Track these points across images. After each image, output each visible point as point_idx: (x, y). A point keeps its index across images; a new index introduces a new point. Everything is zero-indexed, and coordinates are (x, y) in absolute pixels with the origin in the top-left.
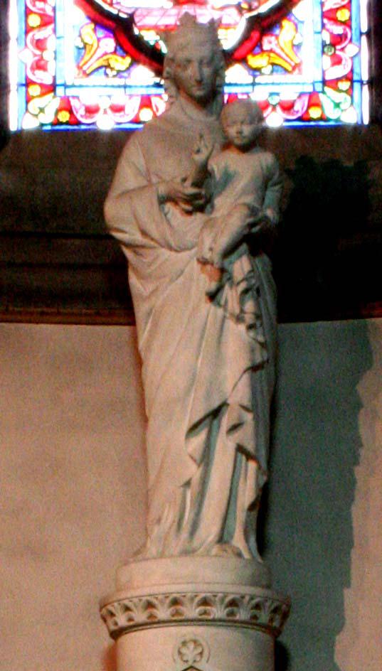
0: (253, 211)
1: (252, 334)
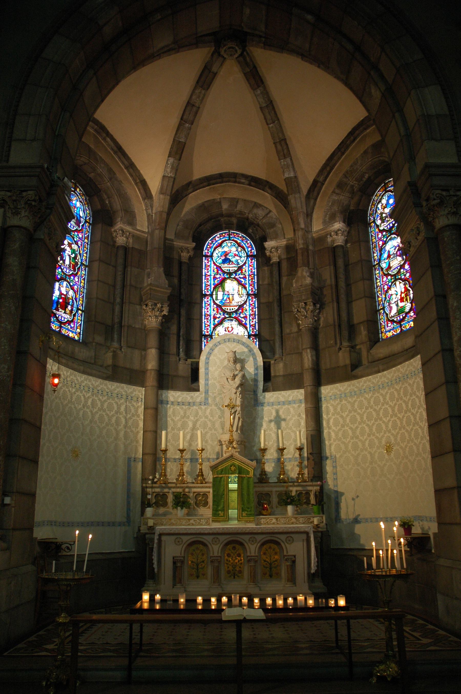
0: (241, 381)
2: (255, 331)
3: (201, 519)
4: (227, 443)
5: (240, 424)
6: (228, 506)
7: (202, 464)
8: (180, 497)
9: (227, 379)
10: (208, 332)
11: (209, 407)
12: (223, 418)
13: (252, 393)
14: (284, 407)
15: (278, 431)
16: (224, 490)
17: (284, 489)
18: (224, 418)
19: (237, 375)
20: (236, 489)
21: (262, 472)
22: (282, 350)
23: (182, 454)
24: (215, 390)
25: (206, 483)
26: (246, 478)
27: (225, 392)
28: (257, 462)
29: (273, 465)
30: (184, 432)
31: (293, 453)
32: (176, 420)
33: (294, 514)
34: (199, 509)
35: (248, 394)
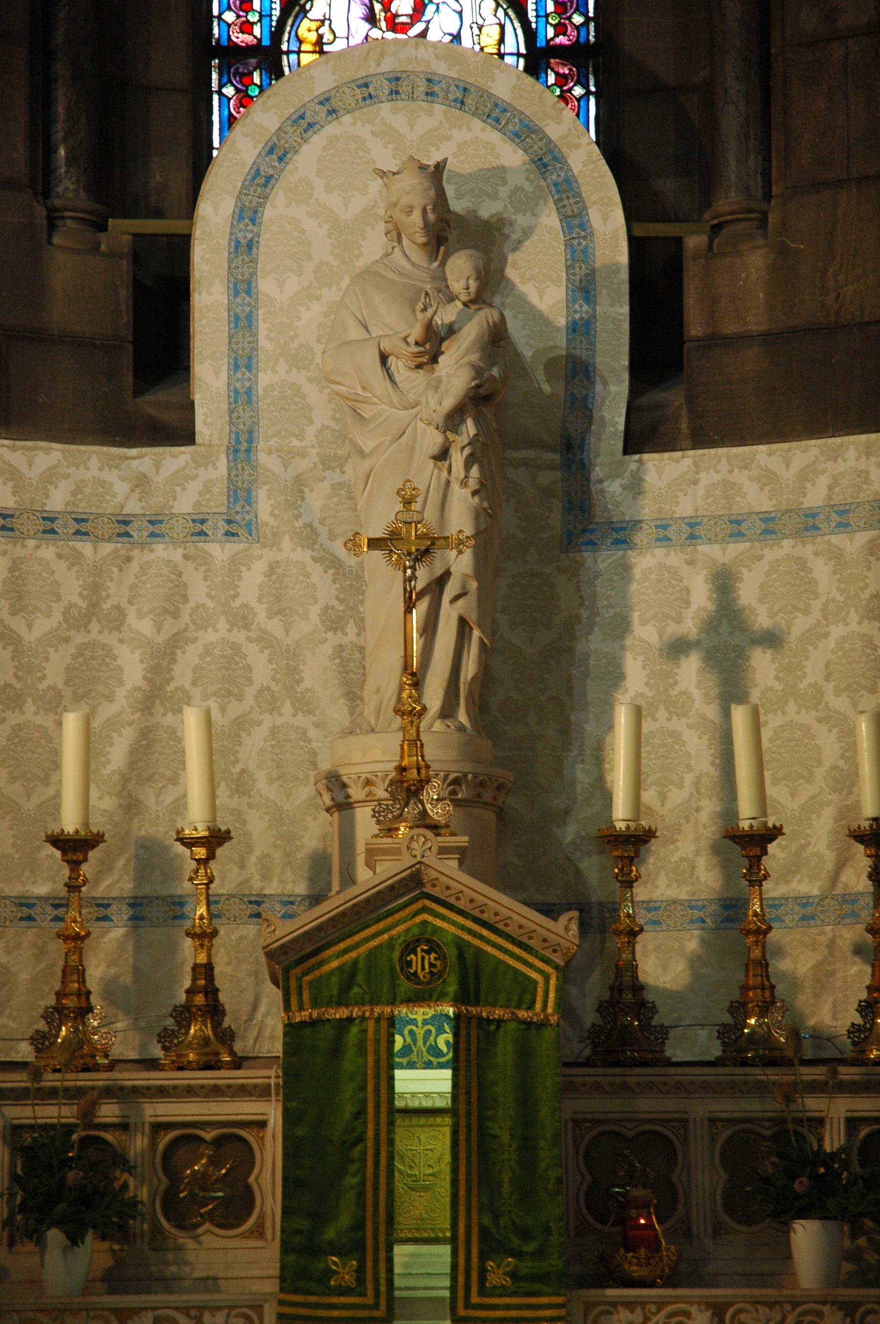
0: (478, 372)
1: (476, 499)
2: (578, 19)
3: (201, 1308)
4: (381, 792)
5: (470, 668)
6: (391, 1219)
7: (215, 933)
8: (66, 1163)
9: (384, 358)
10: (246, 27)
11: (256, 549)
12: (351, 629)
13: (555, 457)
14: (771, 554)
15: (727, 715)
16: (360, 1113)
17: (772, 1106)
18: (361, 624)
19: (451, 330)
20: (445, 1103)
21: (617, 989)
22: (767, 158)
23: (75, 865)
24: (301, 436)
25: (238, 1063)
26: (512, 1025)
27: (367, 446)
28: (583, 926)
29: (692, 945)
30: (87, 722)
31: (830, 866)
32: (30, 637)
33: (833, 1279)
34: (191, 1244)
35: (525, 463)
